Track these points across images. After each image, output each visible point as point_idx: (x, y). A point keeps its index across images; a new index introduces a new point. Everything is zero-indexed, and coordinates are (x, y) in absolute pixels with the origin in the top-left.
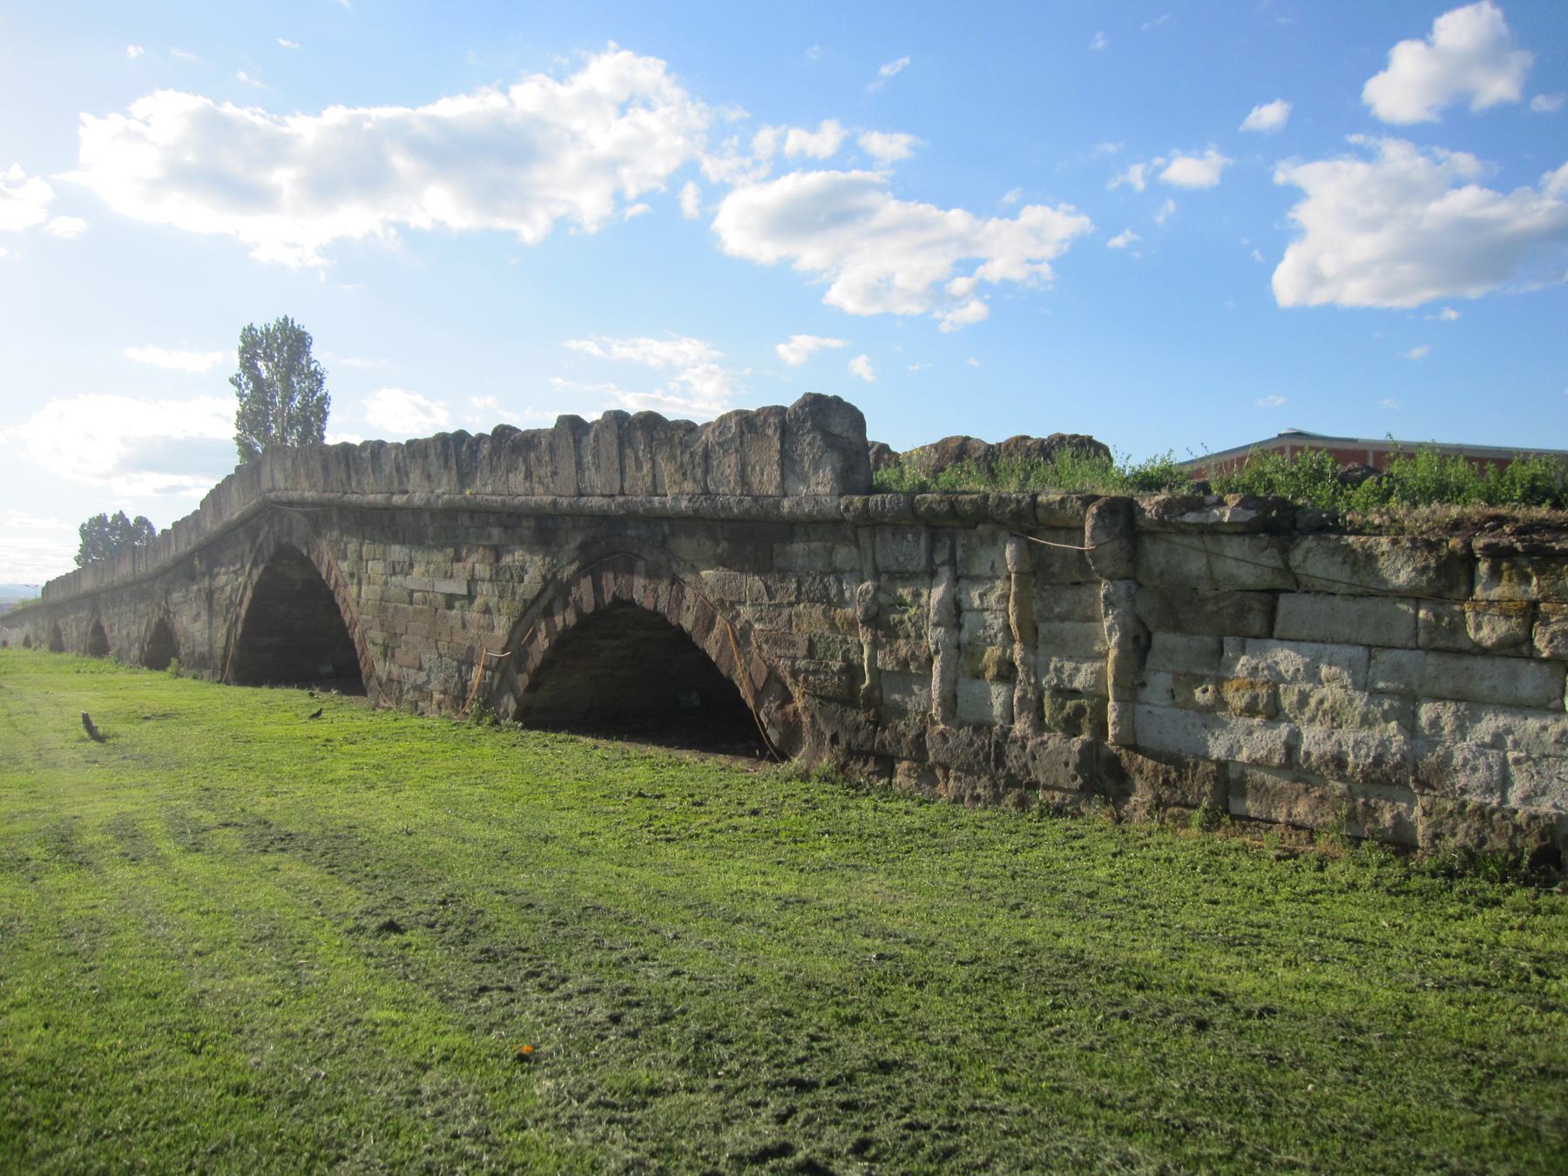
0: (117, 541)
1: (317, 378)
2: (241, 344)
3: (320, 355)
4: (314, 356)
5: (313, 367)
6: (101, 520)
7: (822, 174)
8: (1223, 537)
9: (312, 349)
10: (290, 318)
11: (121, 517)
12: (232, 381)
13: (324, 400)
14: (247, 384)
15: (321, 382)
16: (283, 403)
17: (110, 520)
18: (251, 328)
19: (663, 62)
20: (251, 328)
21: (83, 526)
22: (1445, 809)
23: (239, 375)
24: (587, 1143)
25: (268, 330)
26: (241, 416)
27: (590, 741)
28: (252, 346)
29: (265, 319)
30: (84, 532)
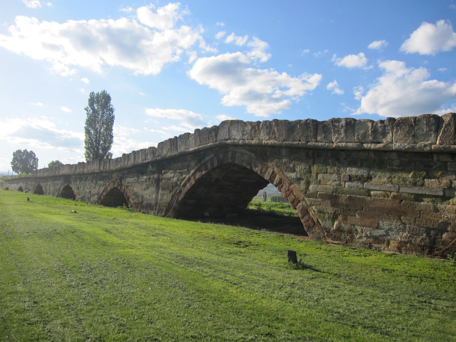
0: (24, 158)
1: (112, 110)
2: (90, 98)
3: (113, 103)
4: (111, 103)
5: (111, 107)
6: (19, 151)
7: (252, 69)
8: (453, 190)
9: (111, 101)
10: (106, 91)
11: (26, 151)
12: (85, 109)
13: (113, 117)
14: (90, 111)
15: (113, 112)
16: (101, 118)
17: (22, 151)
18: (93, 93)
19: (305, 73)
20: (93, 93)
21: (14, 153)
22: (78, 277)
23: (88, 107)
24: (325, 315)
25: (98, 94)
26: (88, 121)
27: (248, 229)
28: (93, 100)
29: (98, 90)
30: (14, 154)
